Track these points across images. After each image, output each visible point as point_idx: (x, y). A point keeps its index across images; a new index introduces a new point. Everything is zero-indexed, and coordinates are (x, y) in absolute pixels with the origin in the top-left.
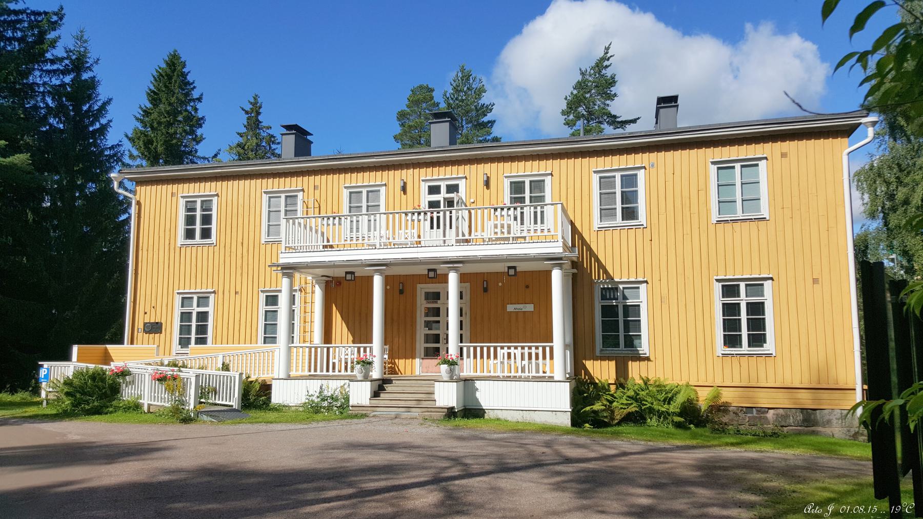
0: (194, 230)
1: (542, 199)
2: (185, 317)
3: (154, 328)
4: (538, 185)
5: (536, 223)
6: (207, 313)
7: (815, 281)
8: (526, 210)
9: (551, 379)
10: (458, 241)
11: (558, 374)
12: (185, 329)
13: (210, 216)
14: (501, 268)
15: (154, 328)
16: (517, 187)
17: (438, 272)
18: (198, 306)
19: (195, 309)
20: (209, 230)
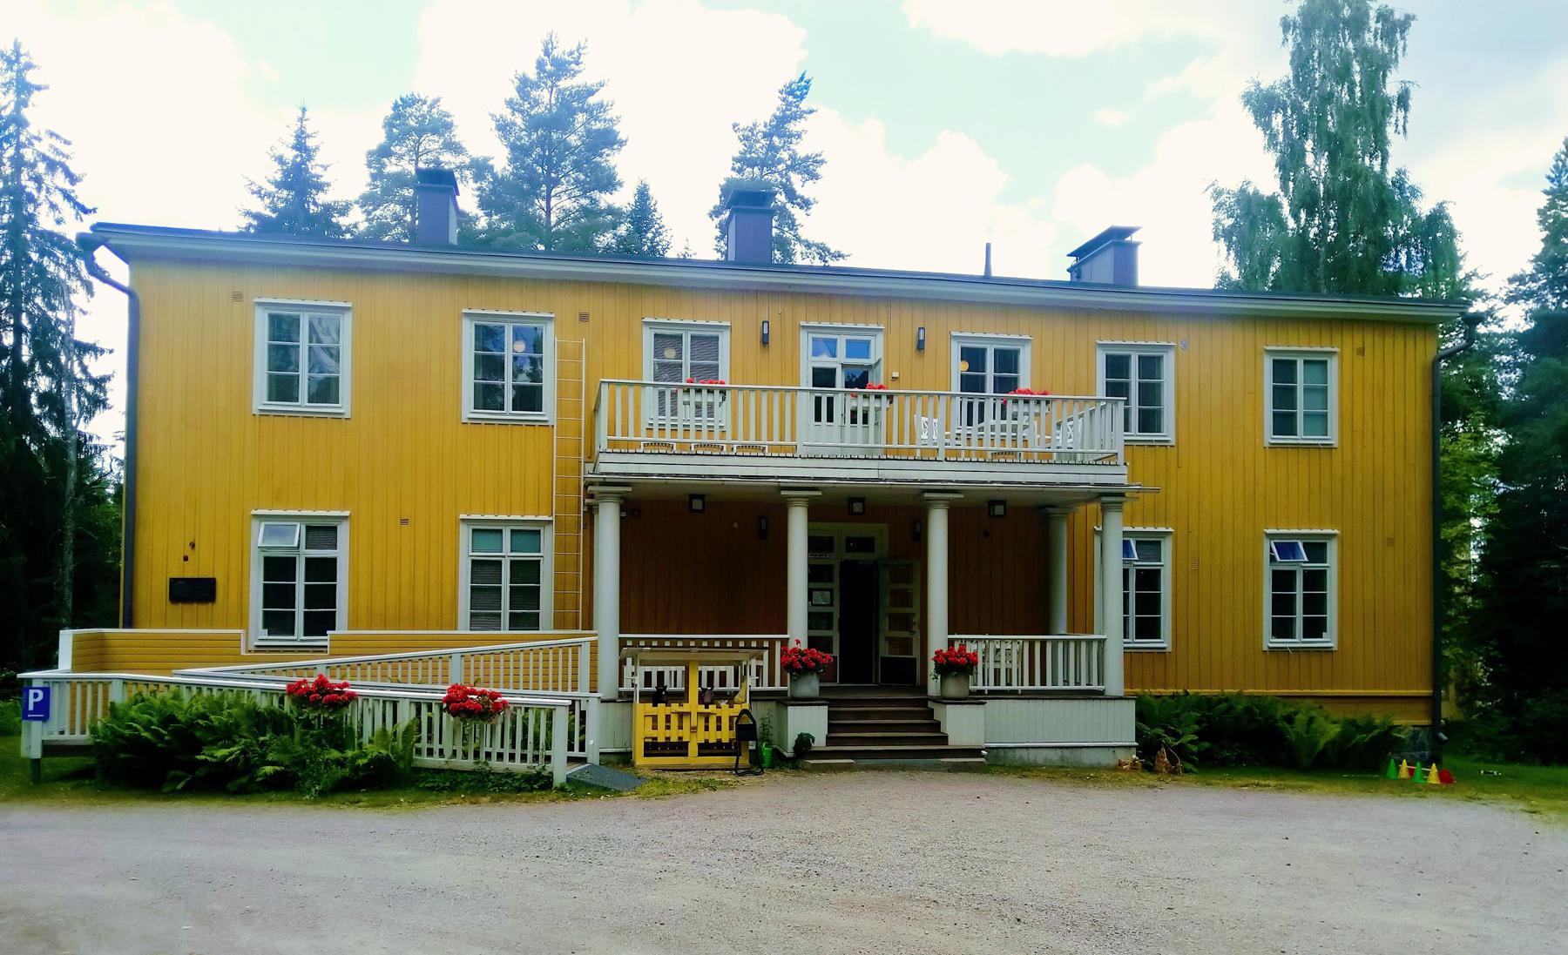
3: (194, 592)
11: (1114, 682)
15: (194, 592)
16: (973, 356)
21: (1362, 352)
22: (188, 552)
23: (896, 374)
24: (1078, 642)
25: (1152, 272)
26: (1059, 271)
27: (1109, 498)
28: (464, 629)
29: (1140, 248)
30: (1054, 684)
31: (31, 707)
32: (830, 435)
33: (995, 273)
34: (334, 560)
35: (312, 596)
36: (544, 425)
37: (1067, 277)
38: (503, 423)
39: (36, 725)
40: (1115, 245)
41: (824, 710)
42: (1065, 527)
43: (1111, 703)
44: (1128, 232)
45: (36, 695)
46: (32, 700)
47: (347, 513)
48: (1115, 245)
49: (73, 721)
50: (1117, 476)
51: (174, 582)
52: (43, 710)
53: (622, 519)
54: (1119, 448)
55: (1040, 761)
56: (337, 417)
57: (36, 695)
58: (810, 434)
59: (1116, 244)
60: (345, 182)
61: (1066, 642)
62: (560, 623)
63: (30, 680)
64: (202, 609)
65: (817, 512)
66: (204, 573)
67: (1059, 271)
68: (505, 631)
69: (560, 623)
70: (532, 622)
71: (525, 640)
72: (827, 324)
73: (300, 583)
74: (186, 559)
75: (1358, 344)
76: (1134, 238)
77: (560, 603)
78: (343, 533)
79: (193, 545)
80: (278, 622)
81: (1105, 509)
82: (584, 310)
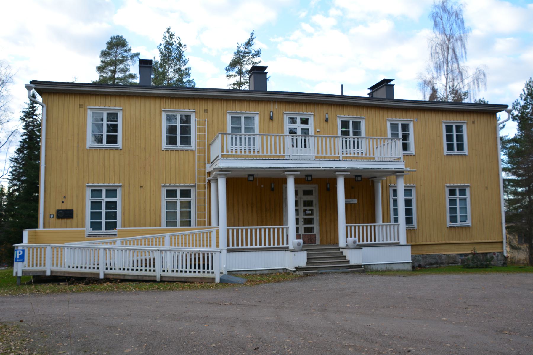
0: (453, 145)
1: (252, 129)
2: (96, 205)
3: (65, 215)
4: (356, 125)
5: (354, 148)
6: (115, 203)
7: (487, 188)
8: (243, 137)
9: (397, 244)
10: (223, 156)
11: (403, 240)
12: (96, 215)
13: (116, 126)
14: (244, 175)
15: (65, 215)
16: (345, 124)
17: (313, 177)
18: (460, 199)
19: (104, 199)
20: (462, 145)
21: (474, 122)
22: (64, 200)
23: (318, 130)
24: (387, 225)
25: (401, 93)
26: (365, 93)
27: (398, 173)
28: (164, 227)
29: (394, 86)
30: (379, 241)
31: (18, 257)
32: (301, 152)
33: (344, 94)
34: (116, 202)
35: (108, 216)
36: (192, 150)
37: (368, 96)
38: (177, 150)
39: (20, 264)
40: (386, 85)
41: (305, 253)
42: (380, 185)
43: (403, 247)
44: (391, 80)
45: (20, 253)
46: (18, 255)
47: (120, 185)
48: (386, 85)
49: (29, 263)
50: (401, 166)
51: (58, 211)
52: (22, 258)
53: (271, 178)
54: (401, 156)
55: (379, 269)
56: (117, 149)
57: (20, 253)
58: (289, 151)
59: (385, 85)
60: (441, 94)
61: (383, 225)
62: (199, 224)
63: (17, 247)
64: (68, 221)
65: (297, 181)
66: (69, 208)
67: (365, 93)
68: (178, 227)
69: (199, 224)
70: (189, 224)
71: (186, 231)
72: (297, 113)
73: (104, 211)
74: (63, 202)
75: (472, 120)
76: (392, 83)
77: (199, 216)
78: (119, 192)
79: (65, 197)
80: (96, 226)
81: (397, 177)
82: (206, 108)
